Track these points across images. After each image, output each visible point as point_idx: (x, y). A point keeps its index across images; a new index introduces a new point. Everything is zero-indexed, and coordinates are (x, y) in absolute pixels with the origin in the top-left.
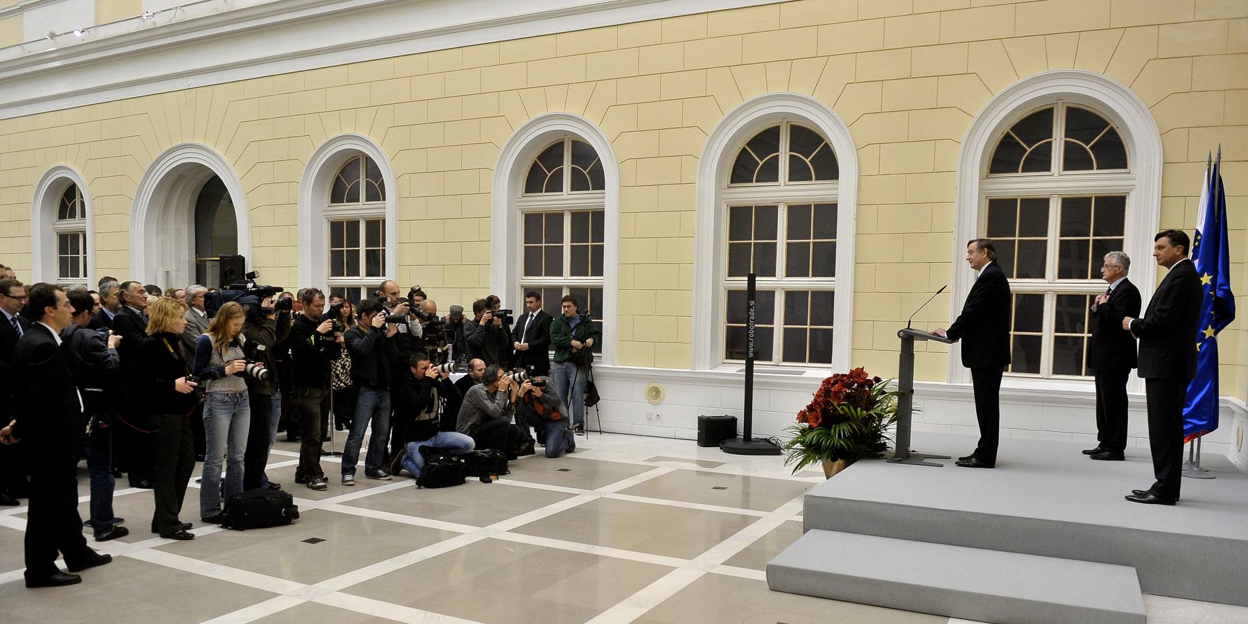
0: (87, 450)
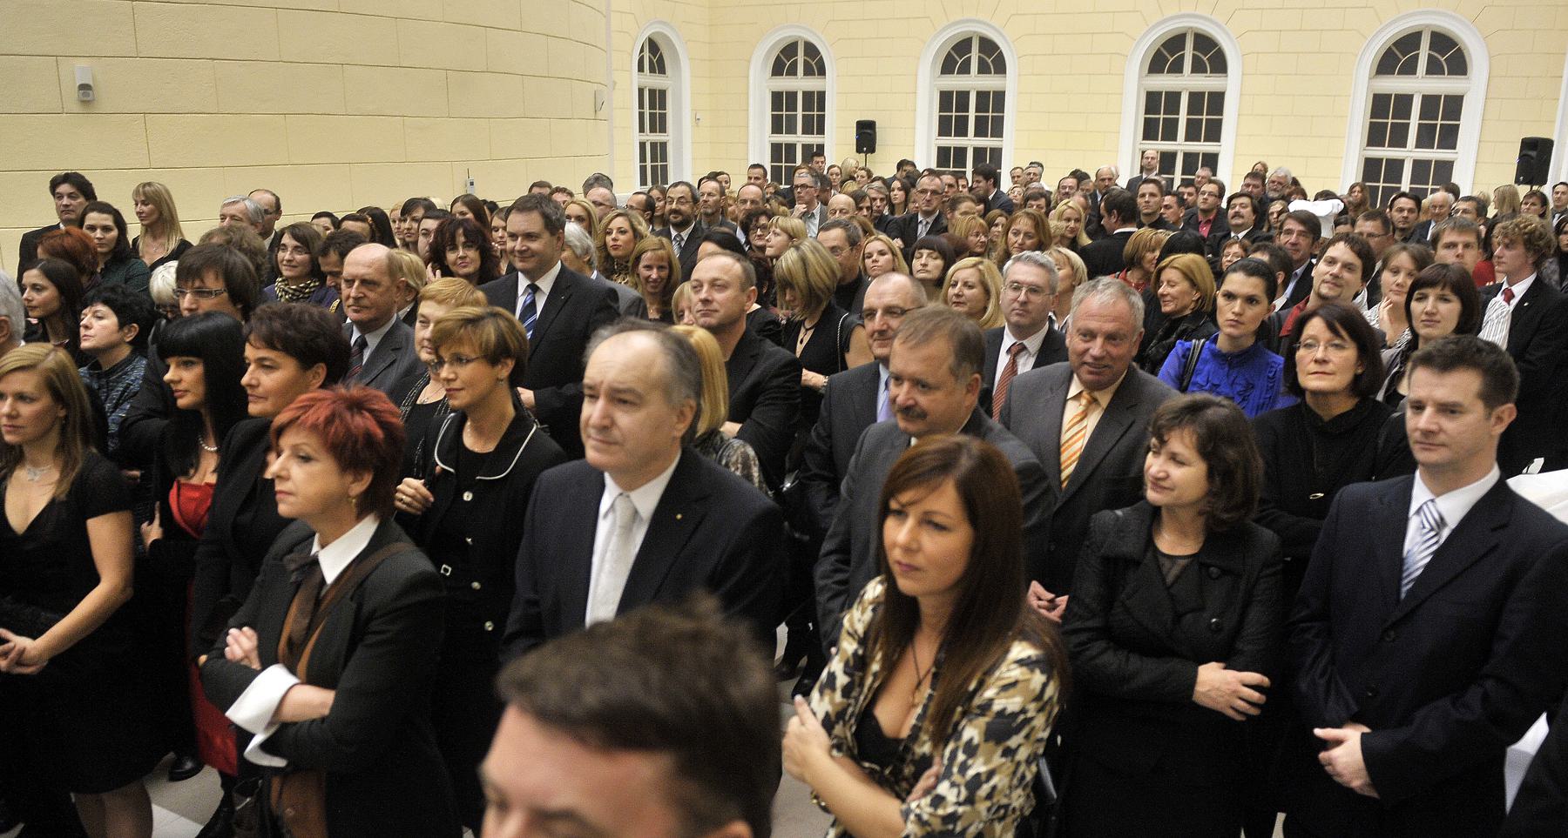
0: (1380, 397)
